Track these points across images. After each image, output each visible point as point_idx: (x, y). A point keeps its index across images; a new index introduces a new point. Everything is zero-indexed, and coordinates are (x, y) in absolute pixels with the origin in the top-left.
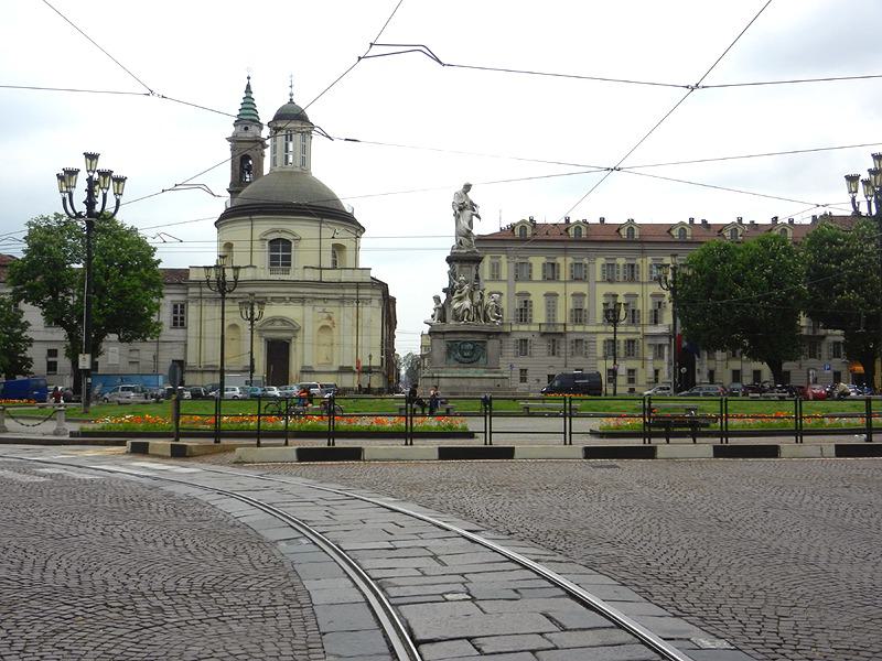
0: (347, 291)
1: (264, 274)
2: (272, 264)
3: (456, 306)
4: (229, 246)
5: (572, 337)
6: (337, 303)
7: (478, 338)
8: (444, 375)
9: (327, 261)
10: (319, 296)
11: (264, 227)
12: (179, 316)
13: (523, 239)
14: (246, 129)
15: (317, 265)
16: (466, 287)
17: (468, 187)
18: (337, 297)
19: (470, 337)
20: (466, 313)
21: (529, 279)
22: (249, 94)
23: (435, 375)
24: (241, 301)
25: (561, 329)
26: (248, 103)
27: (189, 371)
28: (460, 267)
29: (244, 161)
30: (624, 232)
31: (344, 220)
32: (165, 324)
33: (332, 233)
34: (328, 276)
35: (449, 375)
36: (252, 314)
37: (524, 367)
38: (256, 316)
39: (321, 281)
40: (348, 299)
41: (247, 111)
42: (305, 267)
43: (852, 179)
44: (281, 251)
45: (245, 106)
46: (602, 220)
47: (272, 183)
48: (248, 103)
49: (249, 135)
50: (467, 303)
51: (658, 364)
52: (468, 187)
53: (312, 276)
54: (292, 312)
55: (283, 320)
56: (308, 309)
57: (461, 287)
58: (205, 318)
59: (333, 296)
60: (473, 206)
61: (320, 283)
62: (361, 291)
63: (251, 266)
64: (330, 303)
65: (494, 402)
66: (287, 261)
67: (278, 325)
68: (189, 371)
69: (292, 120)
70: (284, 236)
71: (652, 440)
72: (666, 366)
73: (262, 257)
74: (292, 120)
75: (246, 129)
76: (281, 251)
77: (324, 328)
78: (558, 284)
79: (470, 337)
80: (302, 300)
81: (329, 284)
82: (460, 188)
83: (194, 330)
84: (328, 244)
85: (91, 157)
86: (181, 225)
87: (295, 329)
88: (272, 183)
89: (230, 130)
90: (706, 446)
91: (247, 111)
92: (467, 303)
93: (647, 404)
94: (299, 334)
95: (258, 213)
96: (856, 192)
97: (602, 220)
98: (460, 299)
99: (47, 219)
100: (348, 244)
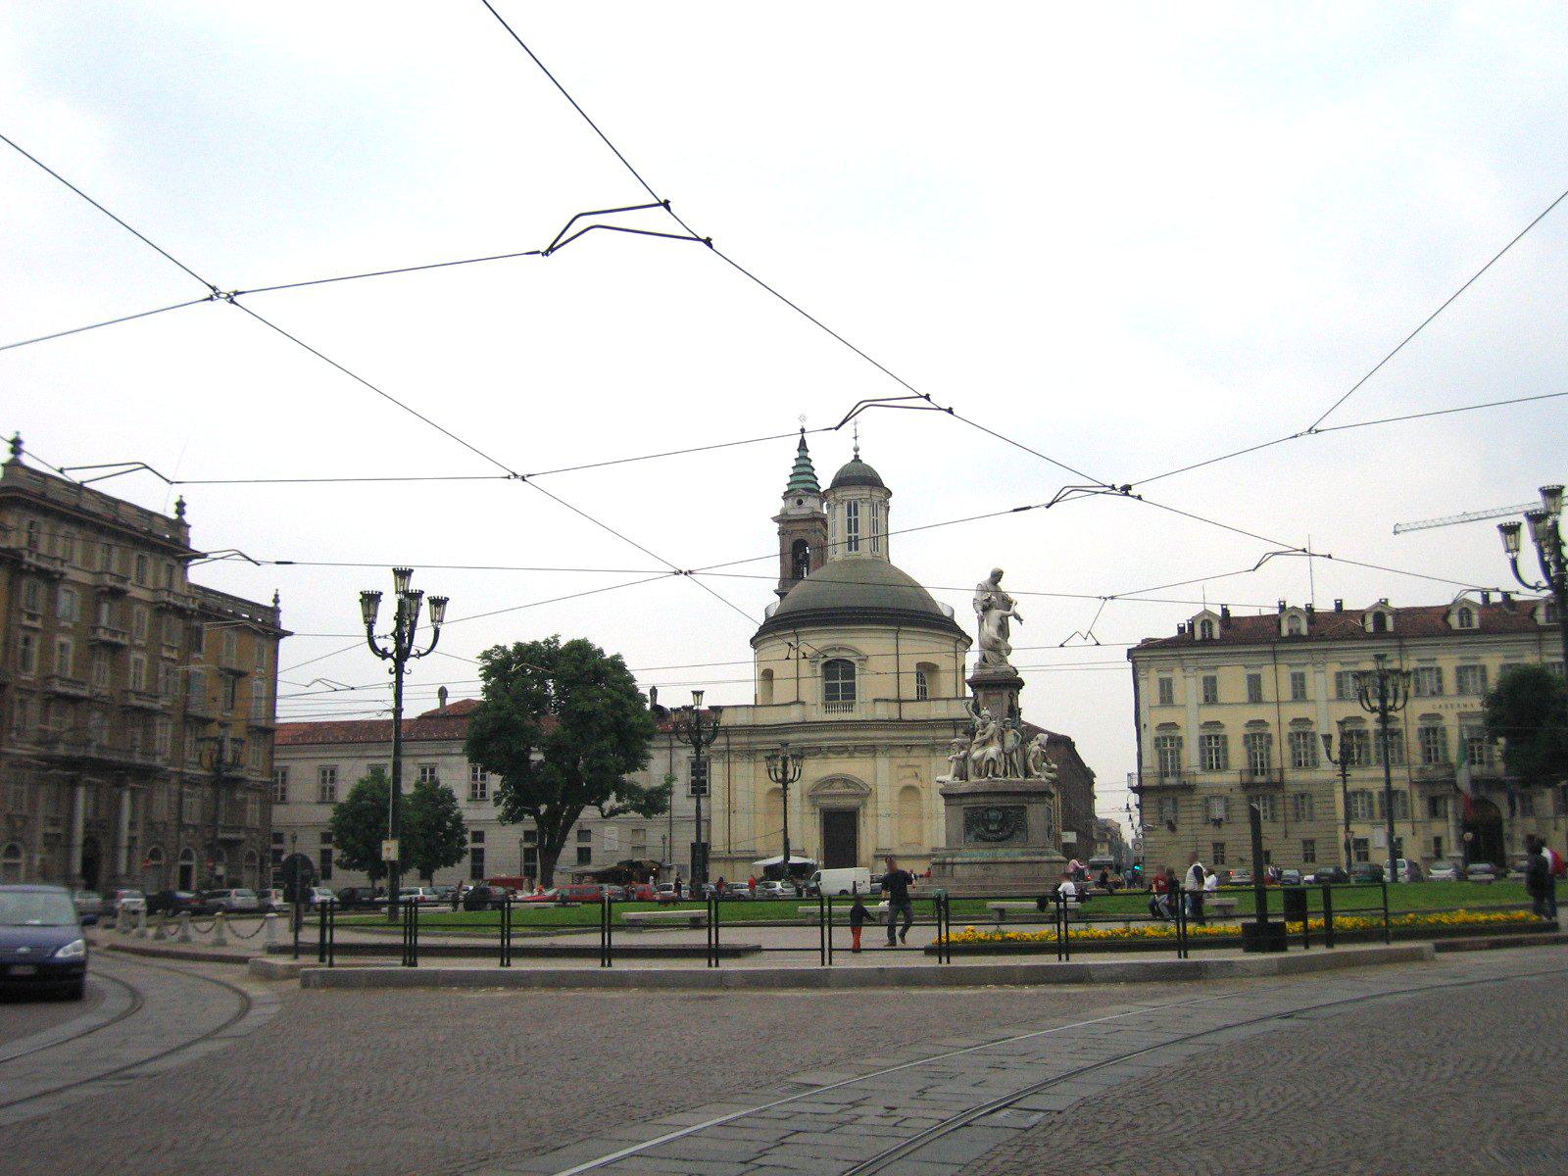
0: (940, 733)
1: (817, 714)
2: (828, 698)
3: (977, 754)
4: (768, 676)
5: (1291, 790)
6: (926, 752)
7: (1008, 802)
8: (959, 860)
9: (910, 689)
10: (900, 742)
11: (817, 641)
12: (479, 782)
13: (1208, 641)
14: (800, 502)
15: (894, 696)
16: (992, 725)
17: (997, 576)
18: (925, 742)
19: (996, 801)
20: (991, 766)
21: (1438, 692)
22: (803, 453)
23: (949, 860)
24: (768, 754)
25: (1276, 777)
26: (803, 467)
27: (714, 860)
28: (985, 694)
29: (800, 546)
30: (1454, 621)
31: (940, 627)
32: (456, 794)
33: (918, 647)
34: (912, 711)
35: (967, 860)
36: (785, 773)
37: (1309, 836)
38: (790, 776)
39: (900, 720)
40: (942, 745)
41: (800, 478)
42: (876, 700)
43: (1510, 530)
44: (839, 677)
45: (797, 470)
46: (1339, 605)
47: (833, 571)
48: (803, 467)
49: (805, 511)
50: (992, 750)
51: (1438, 828)
52: (997, 576)
53: (882, 712)
54: (856, 767)
55: (846, 781)
56: (883, 764)
57: (984, 725)
58: (739, 786)
59: (921, 742)
60: (1007, 603)
61: (900, 723)
62: (732, 739)
63: (798, 702)
64: (915, 752)
65: (952, 904)
66: (850, 692)
67: (838, 788)
68: (714, 860)
69: (860, 479)
70: (843, 655)
71: (1071, 956)
72: (1452, 832)
73: (813, 689)
74: (860, 479)
75: (800, 502)
76: (839, 677)
77: (909, 789)
78: (1265, 707)
79: (996, 801)
80: (872, 750)
81: (914, 724)
82: (986, 577)
83: (720, 800)
84: (909, 665)
85: (403, 574)
86: (694, 640)
87: (864, 793)
88: (833, 571)
89: (777, 506)
90: (245, 968)
91: (800, 478)
92: (992, 750)
93: (826, 907)
94: (870, 801)
95: (804, 625)
96: (1518, 550)
97: (1339, 605)
98: (984, 744)
99: (503, 649)
100: (945, 663)
